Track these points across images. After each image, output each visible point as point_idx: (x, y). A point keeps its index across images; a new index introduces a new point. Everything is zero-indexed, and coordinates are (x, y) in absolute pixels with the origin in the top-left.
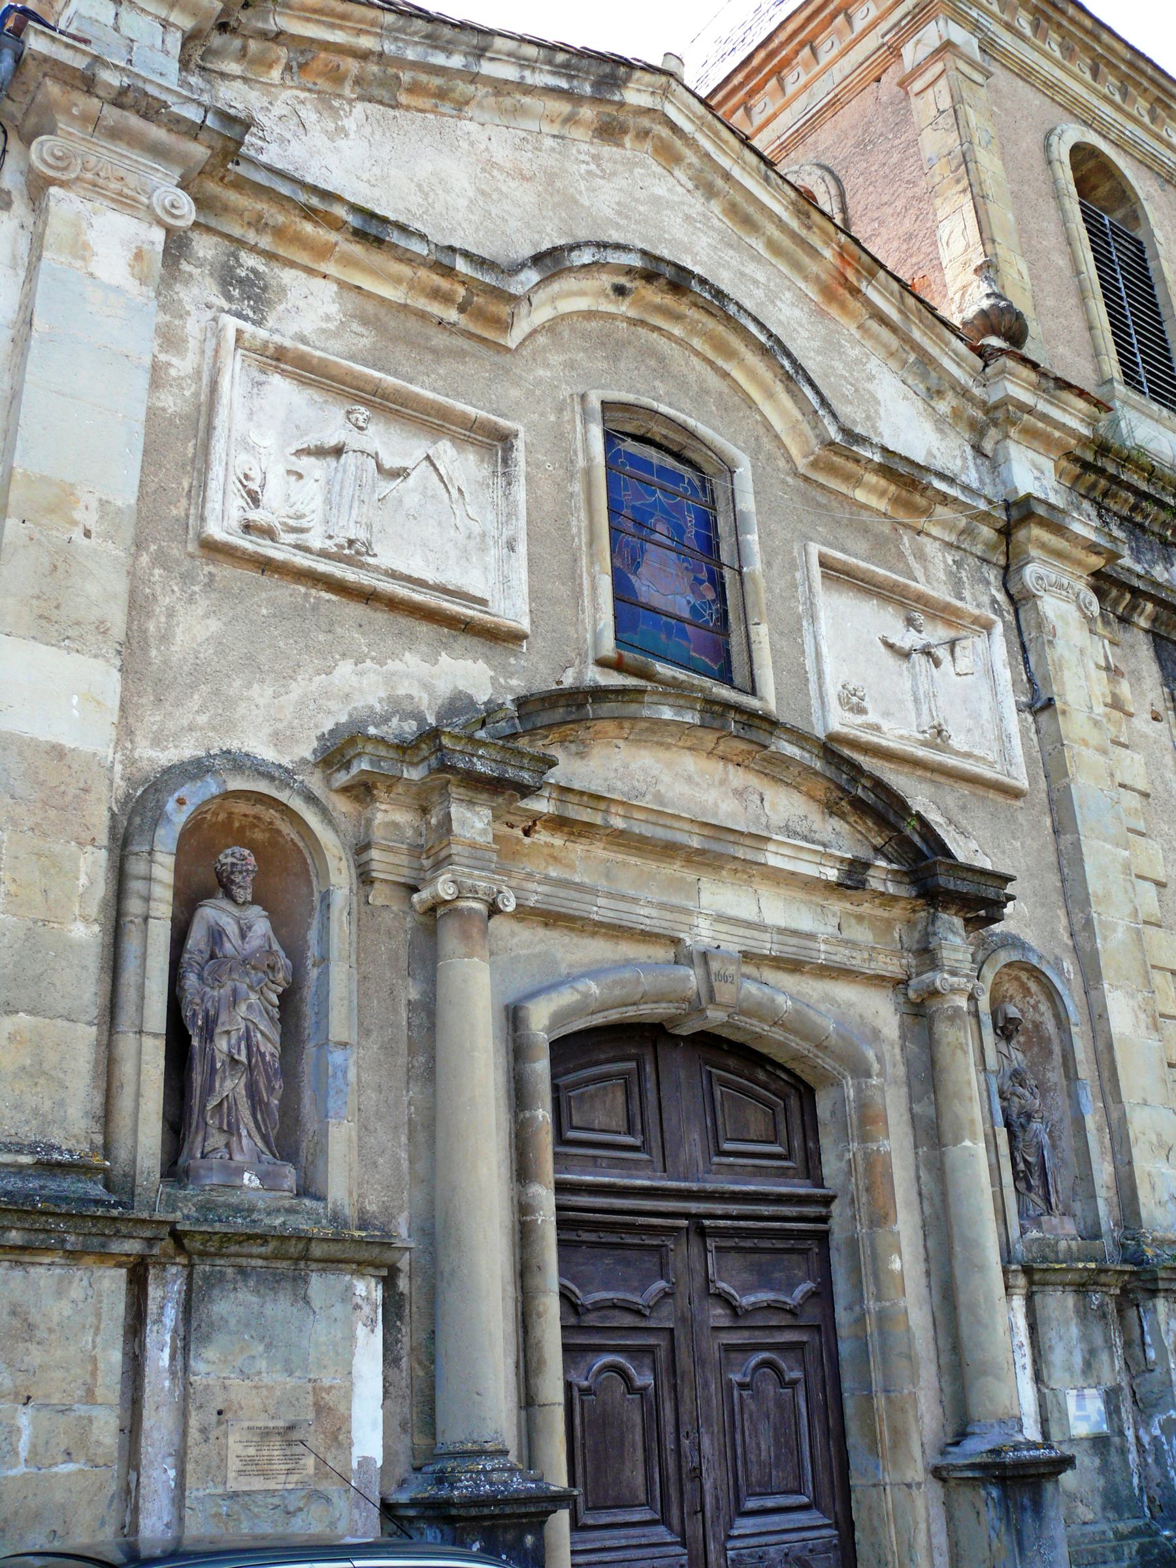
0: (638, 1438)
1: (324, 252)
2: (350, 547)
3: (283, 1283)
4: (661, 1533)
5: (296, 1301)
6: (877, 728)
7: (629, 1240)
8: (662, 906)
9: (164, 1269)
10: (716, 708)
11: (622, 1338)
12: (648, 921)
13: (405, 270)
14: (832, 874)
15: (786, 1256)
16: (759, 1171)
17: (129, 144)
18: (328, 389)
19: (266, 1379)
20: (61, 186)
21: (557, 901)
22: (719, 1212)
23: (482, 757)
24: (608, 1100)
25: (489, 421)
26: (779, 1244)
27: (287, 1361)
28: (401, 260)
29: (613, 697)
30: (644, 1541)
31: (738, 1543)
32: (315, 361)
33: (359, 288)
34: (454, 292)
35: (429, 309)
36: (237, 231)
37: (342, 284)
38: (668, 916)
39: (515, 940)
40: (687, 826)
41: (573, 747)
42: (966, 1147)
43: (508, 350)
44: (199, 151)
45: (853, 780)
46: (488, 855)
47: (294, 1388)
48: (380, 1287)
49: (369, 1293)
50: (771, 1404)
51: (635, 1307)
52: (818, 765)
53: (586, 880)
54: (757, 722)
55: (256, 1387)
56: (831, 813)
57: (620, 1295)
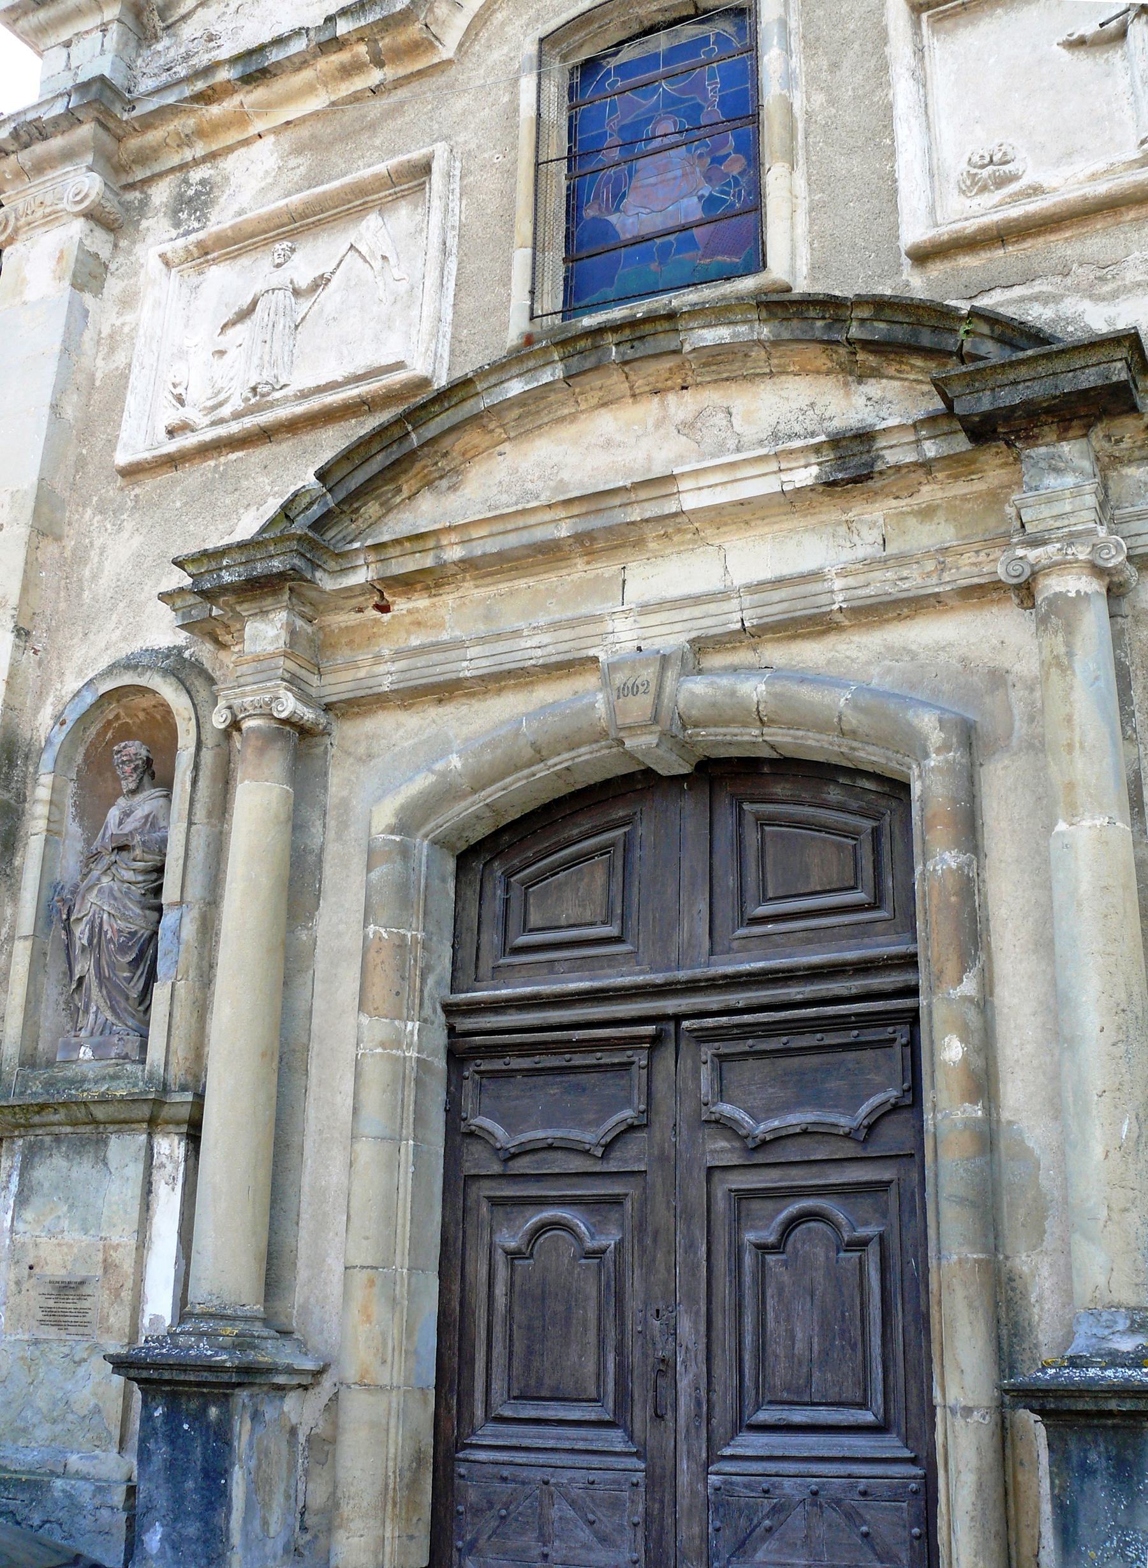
0: (592, 1315)
1: (241, 119)
2: (255, 395)
3: (88, 1147)
4: (615, 1439)
5: (97, 1163)
6: (1036, 190)
7: (578, 1060)
8: (555, 626)
9: (13, 1143)
10: (582, 344)
11: (573, 1187)
12: (539, 652)
13: (307, 74)
14: (805, 475)
15: (850, 1056)
16: (814, 937)
17: (51, 168)
18: (255, 247)
19: (68, 1237)
20: (11, 244)
21: (415, 673)
22: (715, 1007)
23: (228, 567)
24: (582, 885)
25: (401, 164)
26: (831, 1039)
27: (84, 1220)
28: (299, 69)
29: (437, 408)
30: (580, 1445)
31: (728, 1467)
32: (230, 233)
33: (288, 123)
34: (356, 56)
35: (353, 89)
36: (175, 160)
37: (276, 131)
38: (567, 634)
39: (401, 732)
40: (548, 516)
41: (444, 483)
42: (1062, 834)
43: (450, 62)
44: (87, 130)
45: (838, 321)
46: (273, 663)
47: (88, 1245)
48: (183, 1144)
49: (172, 1151)
50: (819, 1276)
51: (580, 1147)
52: (765, 332)
53: (458, 633)
54: (648, 328)
55: (59, 1245)
56: (860, 380)
57: (559, 1134)
